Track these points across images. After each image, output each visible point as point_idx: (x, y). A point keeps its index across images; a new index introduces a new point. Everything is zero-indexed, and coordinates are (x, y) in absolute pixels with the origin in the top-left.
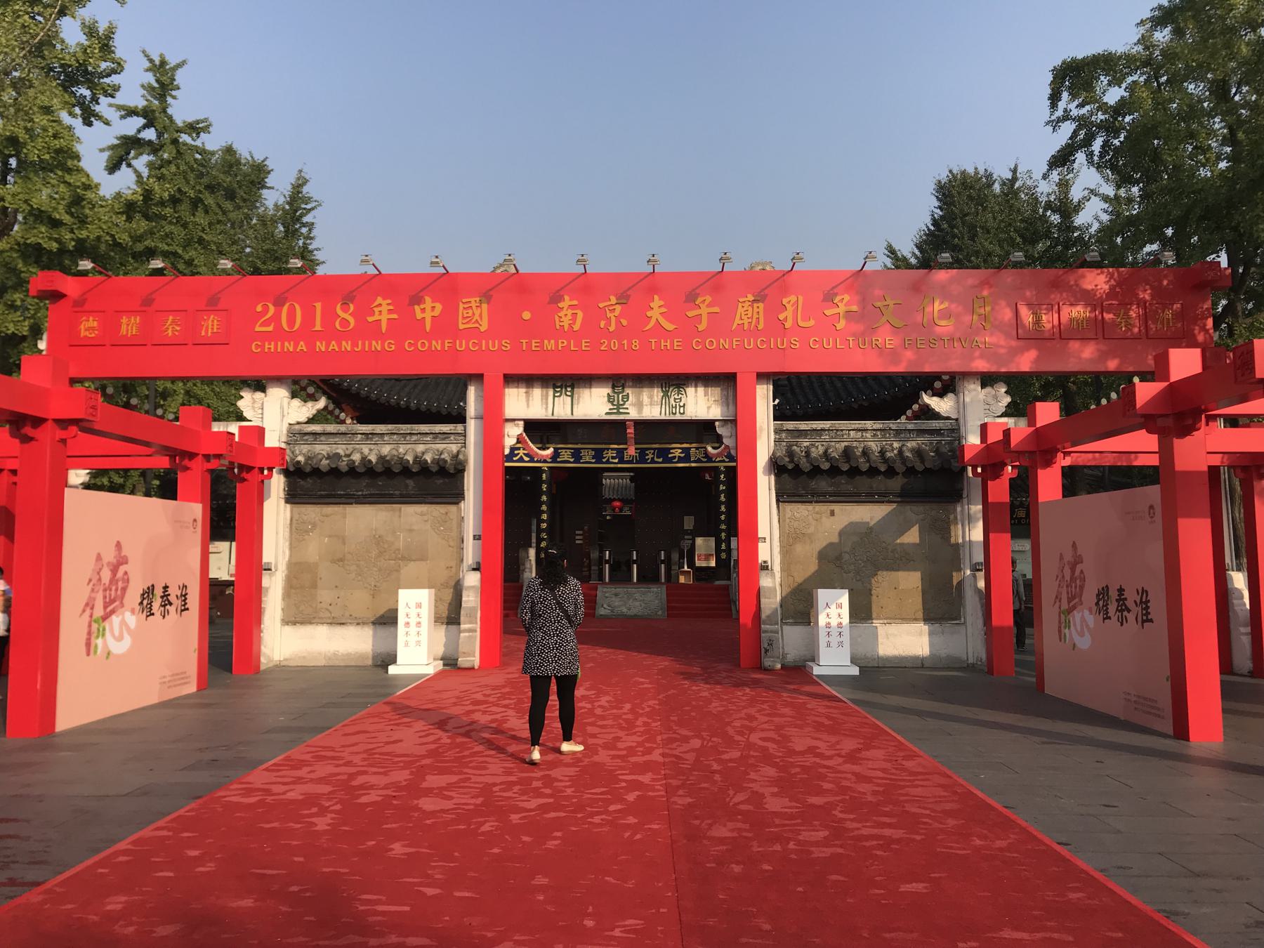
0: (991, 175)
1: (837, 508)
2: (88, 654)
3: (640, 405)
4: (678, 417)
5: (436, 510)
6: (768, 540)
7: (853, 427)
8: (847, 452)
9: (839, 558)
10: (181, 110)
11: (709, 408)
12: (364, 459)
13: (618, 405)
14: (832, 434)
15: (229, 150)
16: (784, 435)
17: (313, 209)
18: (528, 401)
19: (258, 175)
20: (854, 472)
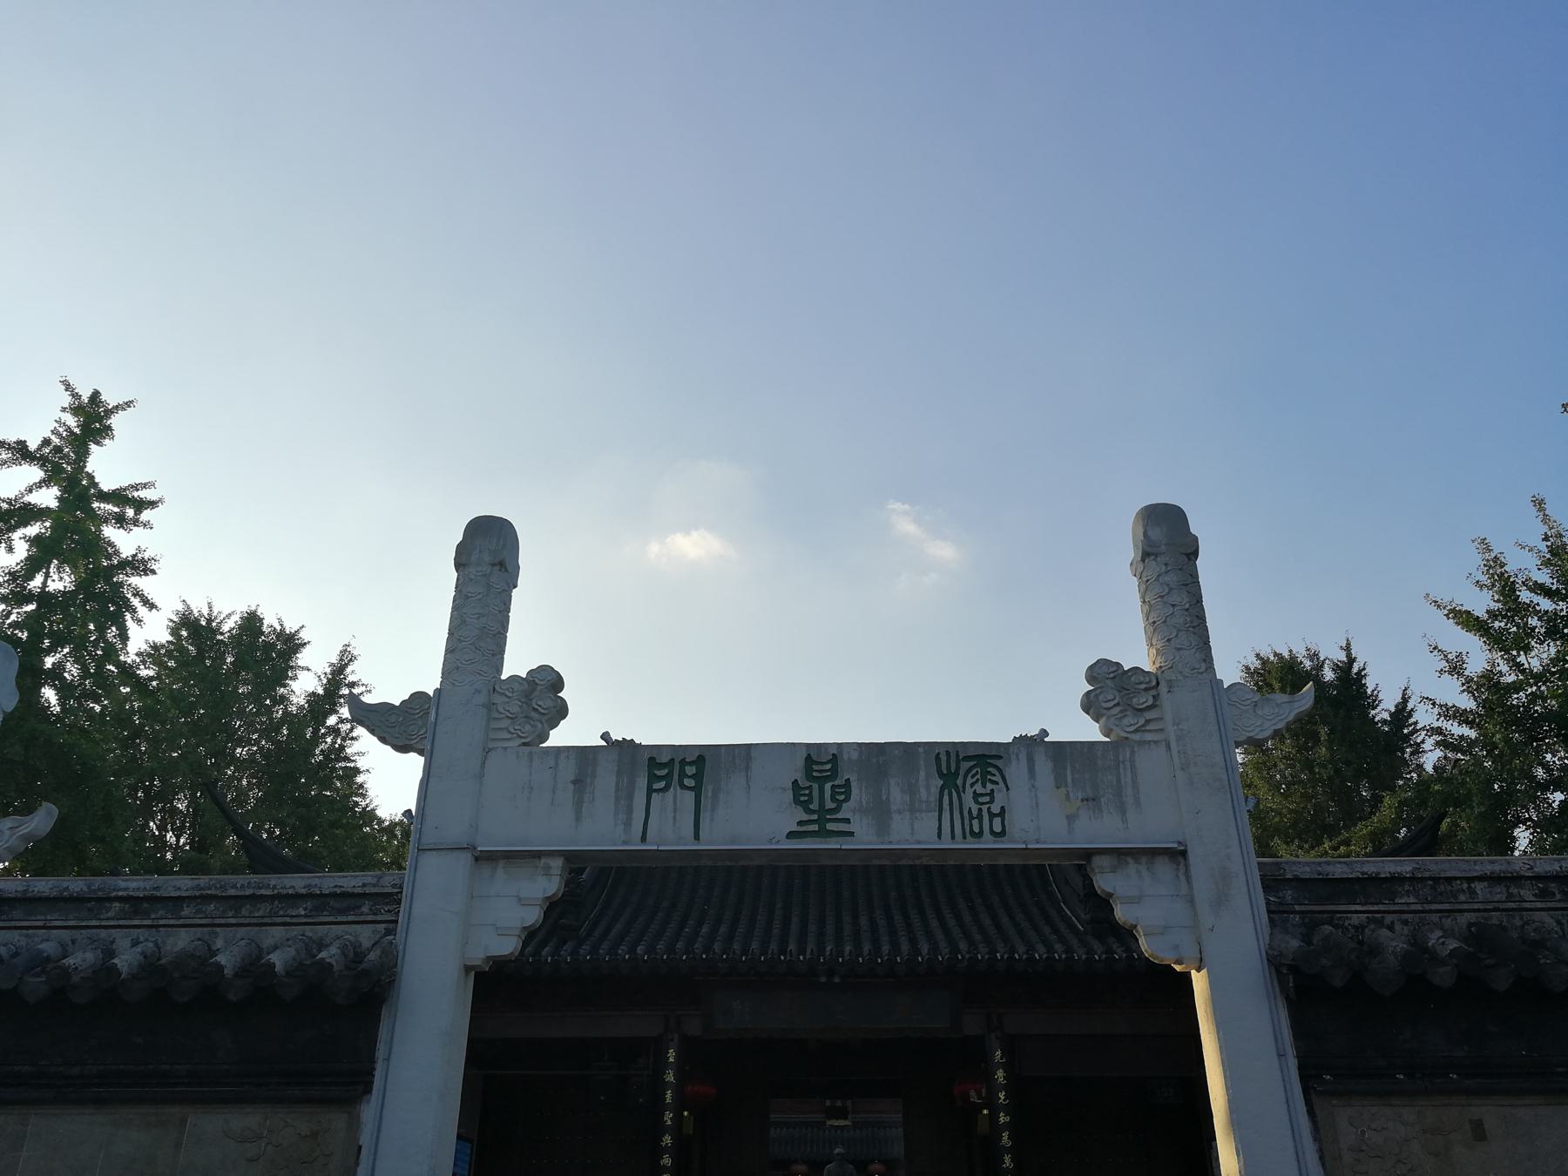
0: (1316, 655)
1: (1490, 1112)
3: (881, 813)
4: (987, 843)
7: (1478, 870)
10: (107, 466)
11: (1071, 818)
12: (105, 970)
13: (822, 810)
15: (252, 622)
16: (1288, 895)
18: (578, 804)
19: (290, 644)
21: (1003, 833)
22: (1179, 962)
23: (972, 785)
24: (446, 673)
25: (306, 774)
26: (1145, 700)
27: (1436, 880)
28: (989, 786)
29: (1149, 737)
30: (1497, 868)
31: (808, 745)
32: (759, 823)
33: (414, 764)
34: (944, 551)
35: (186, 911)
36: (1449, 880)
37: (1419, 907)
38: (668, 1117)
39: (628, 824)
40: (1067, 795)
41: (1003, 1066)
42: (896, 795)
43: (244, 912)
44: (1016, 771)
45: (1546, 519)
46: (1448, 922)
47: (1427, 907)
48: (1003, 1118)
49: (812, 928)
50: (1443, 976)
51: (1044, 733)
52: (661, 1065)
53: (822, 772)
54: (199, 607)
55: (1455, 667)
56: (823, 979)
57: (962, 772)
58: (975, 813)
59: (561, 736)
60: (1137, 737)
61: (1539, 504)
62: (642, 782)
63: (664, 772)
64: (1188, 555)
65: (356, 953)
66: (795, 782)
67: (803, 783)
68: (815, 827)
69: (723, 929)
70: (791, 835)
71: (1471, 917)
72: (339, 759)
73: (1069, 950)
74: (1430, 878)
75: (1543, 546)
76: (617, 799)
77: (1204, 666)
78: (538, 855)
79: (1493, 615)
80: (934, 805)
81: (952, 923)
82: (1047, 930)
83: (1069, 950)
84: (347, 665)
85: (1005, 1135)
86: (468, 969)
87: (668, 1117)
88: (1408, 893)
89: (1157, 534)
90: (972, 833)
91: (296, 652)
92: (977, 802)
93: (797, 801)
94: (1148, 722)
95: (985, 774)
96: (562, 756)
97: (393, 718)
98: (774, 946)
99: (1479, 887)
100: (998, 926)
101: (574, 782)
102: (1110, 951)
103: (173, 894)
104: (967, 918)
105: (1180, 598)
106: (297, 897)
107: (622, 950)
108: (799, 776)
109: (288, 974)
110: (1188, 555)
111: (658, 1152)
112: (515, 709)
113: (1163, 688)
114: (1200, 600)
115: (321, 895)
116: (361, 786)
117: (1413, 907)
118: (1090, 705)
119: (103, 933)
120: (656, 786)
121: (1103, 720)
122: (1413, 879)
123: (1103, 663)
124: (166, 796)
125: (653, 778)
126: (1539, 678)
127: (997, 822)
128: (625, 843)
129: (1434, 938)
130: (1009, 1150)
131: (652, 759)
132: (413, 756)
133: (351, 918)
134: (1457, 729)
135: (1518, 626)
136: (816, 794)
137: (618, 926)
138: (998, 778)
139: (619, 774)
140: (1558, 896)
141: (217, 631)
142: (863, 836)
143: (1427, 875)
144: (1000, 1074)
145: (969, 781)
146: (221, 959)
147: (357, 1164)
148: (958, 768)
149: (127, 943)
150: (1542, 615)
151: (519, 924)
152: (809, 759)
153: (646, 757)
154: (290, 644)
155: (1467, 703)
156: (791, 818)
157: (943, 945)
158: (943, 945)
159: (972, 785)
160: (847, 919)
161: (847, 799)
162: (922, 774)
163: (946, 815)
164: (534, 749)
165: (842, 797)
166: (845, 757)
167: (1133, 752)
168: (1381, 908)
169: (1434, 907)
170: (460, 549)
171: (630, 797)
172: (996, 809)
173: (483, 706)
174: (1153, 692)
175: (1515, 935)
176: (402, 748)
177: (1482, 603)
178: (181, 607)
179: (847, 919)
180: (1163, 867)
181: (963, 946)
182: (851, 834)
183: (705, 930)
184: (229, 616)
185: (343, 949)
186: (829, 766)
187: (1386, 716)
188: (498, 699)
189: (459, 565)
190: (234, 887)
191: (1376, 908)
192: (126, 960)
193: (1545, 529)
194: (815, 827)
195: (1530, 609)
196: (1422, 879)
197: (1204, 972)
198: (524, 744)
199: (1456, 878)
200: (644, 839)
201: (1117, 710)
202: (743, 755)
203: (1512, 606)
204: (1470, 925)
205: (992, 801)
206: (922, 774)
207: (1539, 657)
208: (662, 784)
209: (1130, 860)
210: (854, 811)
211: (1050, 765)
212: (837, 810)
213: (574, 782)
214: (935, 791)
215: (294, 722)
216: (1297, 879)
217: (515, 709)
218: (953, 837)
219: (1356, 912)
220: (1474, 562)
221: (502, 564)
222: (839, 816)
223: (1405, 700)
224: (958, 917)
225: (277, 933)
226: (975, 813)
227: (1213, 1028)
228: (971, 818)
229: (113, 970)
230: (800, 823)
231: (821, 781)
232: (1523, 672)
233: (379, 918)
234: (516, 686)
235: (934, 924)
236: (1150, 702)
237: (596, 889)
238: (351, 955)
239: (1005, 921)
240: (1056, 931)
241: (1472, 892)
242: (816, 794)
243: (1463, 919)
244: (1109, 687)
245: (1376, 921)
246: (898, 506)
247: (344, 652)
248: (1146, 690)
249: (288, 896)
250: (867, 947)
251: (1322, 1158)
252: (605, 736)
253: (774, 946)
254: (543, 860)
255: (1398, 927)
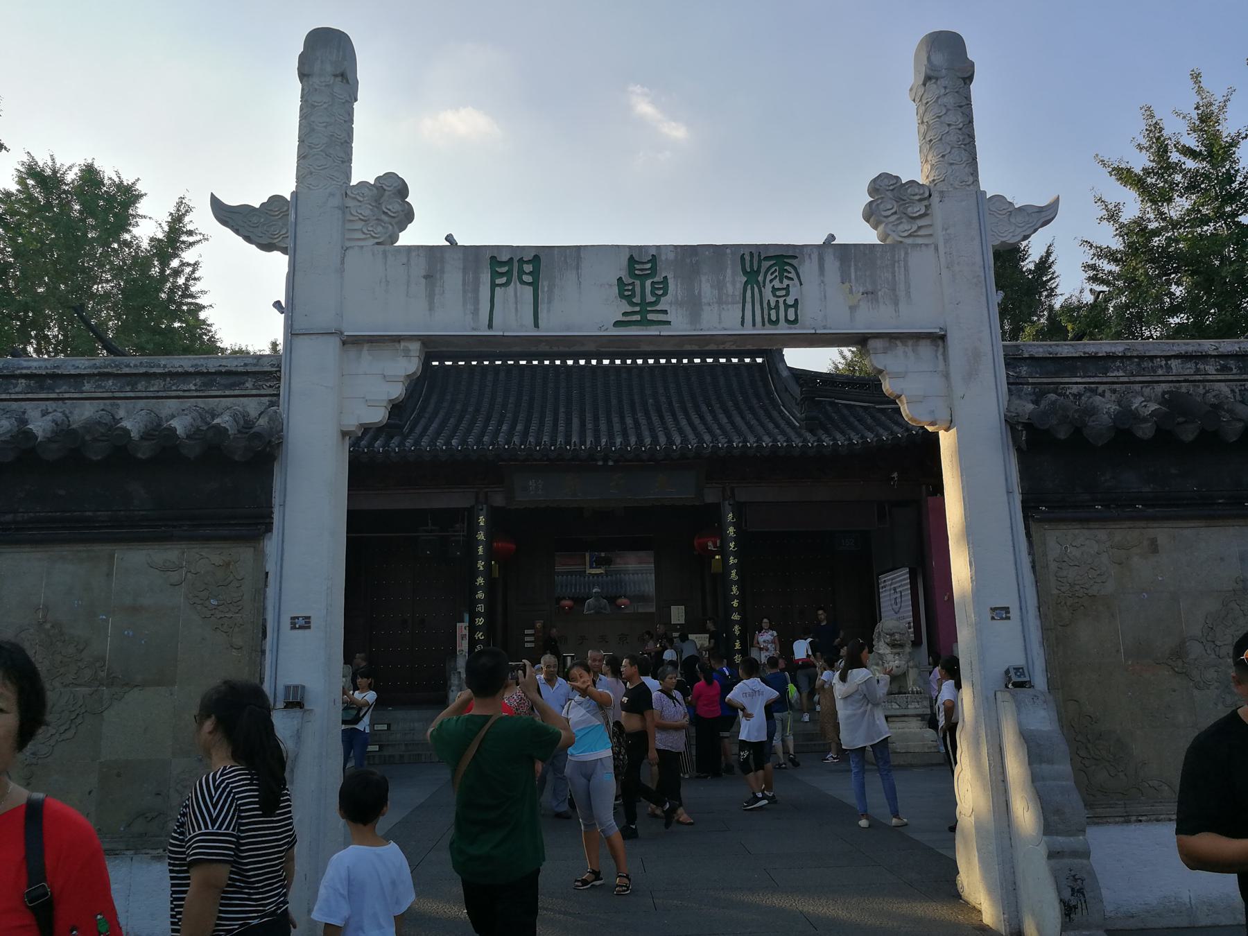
1: (1163, 533)
2: (994, 609)
3: (694, 305)
5: (205, 558)
6: (1015, 613)
8: (1174, 404)
9: (1179, 653)
11: (853, 309)
13: (644, 303)
14: (1132, 367)
15: (90, 175)
16: (1024, 370)
17: (198, 242)
18: (431, 296)
19: (127, 196)
20: (1210, 441)
21: (796, 321)
22: (932, 424)
23: (771, 281)
24: (300, 178)
25: (156, 304)
26: (919, 209)
27: (1142, 358)
28: (786, 282)
29: (920, 241)
30: (1190, 349)
31: (630, 247)
32: (589, 311)
33: (278, 262)
34: (677, 132)
35: (87, 387)
36: (1152, 358)
37: (1126, 379)
38: (481, 565)
39: (476, 312)
40: (851, 291)
41: (734, 524)
42: (706, 289)
43: (140, 387)
44: (808, 269)
45: (1200, 90)
46: (1147, 391)
47: (1132, 379)
48: (732, 561)
49: (589, 426)
50: (1145, 431)
51: (832, 237)
52: (473, 528)
53: (642, 269)
54: (42, 160)
55: (1113, 216)
56: (600, 463)
57: (763, 270)
58: (773, 304)
59: (406, 238)
60: (910, 241)
61: (1196, 77)
62: (486, 278)
63: (504, 269)
64: (964, 79)
65: (245, 421)
66: (620, 279)
67: (627, 280)
68: (638, 318)
69: (519, 427)
70: (617, 324)
71: (1165, 387)
72: (184, 296)
73: (788, 440)
74: (1137, 357)
75: (1194, 114)
76: (465, 292)
77: (971, 179)
78: (398, 339)
79: (1147, 172)
80: (739, 298)
81: (697, 421)
82: (771, 426)
83: (788, 440)
84: (184, 215)
85: (734, 572)
86: (344, 434)
87: (481, 565)
88: (1118, 369)
89: (939, 59)
90: (770, 321)
91: (134, 202)
92: (775, 295)
93: (622, 296)
94: (920, 228)
95: (782, 271)
96: (414, 254)
97: (255, 220)
98: (560, 439)
99: (1174, 363)
100: (732, 423)
101: (426, 277)
102: (820, 440)
103: (73, 372)
104: (709, 418)
105: (956, 118)
106: (186, 375)
107: (440, 442)
108: (623, 274)
109: (188, 437)
110: (964, 79)
111: (474, 590)
112: (367, 212)
113: (935, 199)
114: (971, 122)
115: (208, 373)
116: (204, 322)
117: (1122, 379)
118: (871, 215)
119: (14, 405)
120: (498, 281)
121: (881, 228)
122: (1123, 358)
123: (884, 176)
124: (40, 325)
125: (495, 274)
126: (1175, 225)
127: (791, 312)
128: (474, 329)
129: (1136, 403)
130: (736, 583)
131: (493, 258)
132: (277, 254)
133: (237, 392)
134: (1107, 266)
135: (1166, 181)
136: (638, 289)
137: (435, 425)
138: (793, 275)
139: (465, 270)
140: (1235, 371)
141: (62, 181)
142: (679, 324)
143: (1135, 354)
144: (731, 530)
145: (769, 277)
146: (127, 424)
147: (266, 586)
148: (759, 267)
149: (37, 414)
150: (1185, 173)
151: (385, 397)
152: (631, 259)
153: (488, 256)
154: (127, 196)
155: (1117, 244)
156: (617, 310)
157: (691, 436)
158: (691, 436)
159: (771, 281)
160: (615, 420)
161: (665, 294)
162: (729, 271)
163: (749, 306)
164: (387, 247)
165: (660, 292)
166: (663, 258)
167: (906, 253)
168: (1097, 380)
169: (1138, 379)
170: (303, 59)
171: (476, 291)
172: (790, 301)
173: (338, 208)
174: (926, 203)
175: (1199, 399)
176: (267, 247)
177: (1140, 162)
178: (25, 159)
179: (615, 420)
180: (925, 349)
181: (707, 438)
182: (669, 323)
183: (504, 428)
184: (70, 168)
185: (234, 416)
186: (649, 266)
187: (1032, 266)
188: (350, 203)
189: (303, 75)
190: (128, 366)
191: (1092, 380)
192: (39, 426)
193: (1198, 99)
194: (638, 318)
195: (1175, 168)
196: (1131, 357)
197: (953, 431)
198: (378, 244)
199: (1156, 357)
200: (490, 326)
201: (896, 217)
202: (574, 255)
203: (1165, 167)
204: (1164, 393)
205: (787, 294)
206: (729, 271)
207: (1180, 206)
208: (504, 280)
209: (898, 343)
210: (671, 304)
211: (837, 264)
212: (656, 303)
213: (426, 277)
214: (740, 286)
215: (141, 263)
216: (1032, 358)
217: (367, 212)
218: (754, 325)
219: (1076, 383)
220: (1137, 129)
221: (343, 75)
222: (658, 308)
223: (1048, 254)
224: (702, 418)
225: (172, 405)
226: (773, 304)
227: (957, 473)
228: (770, 308)
229: (30, 435)
230: (625, 314)
231: (643, 278)
232: (1164, 220)
233: (262, 392)
234: (366, 191)
235: (684, 423)
236: (922, 212)
237: (449, 376)
238: (242, 422)
239: (738, 419)
240: (777, 426)
241: (1169, 368)
242: (638, 289)
243: (1160, 388)
244: (889, 197)
245: (1092, 390)
246: (638, 89)
247: (180, 203)
248: (920, 200)
249: (177, 374)
250: (633, 440)
251: (1033, 567)
252: (449, 238)
253: (560, 439)
254: (403, 344)
255: (1108, 394)
